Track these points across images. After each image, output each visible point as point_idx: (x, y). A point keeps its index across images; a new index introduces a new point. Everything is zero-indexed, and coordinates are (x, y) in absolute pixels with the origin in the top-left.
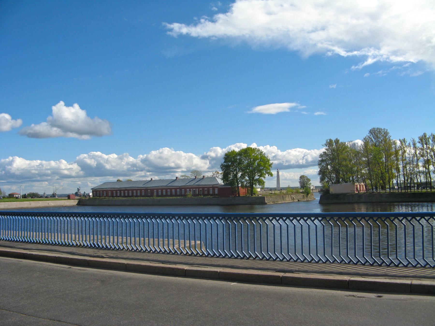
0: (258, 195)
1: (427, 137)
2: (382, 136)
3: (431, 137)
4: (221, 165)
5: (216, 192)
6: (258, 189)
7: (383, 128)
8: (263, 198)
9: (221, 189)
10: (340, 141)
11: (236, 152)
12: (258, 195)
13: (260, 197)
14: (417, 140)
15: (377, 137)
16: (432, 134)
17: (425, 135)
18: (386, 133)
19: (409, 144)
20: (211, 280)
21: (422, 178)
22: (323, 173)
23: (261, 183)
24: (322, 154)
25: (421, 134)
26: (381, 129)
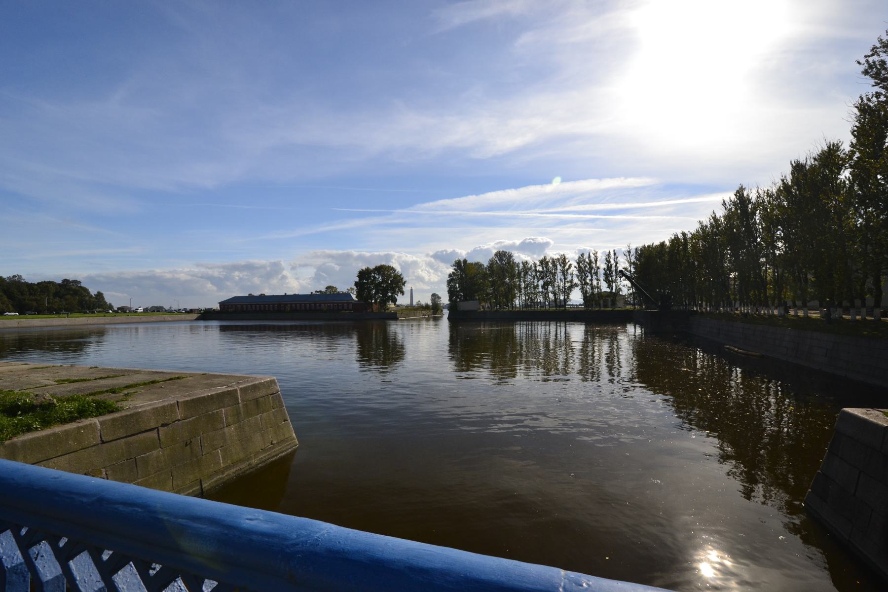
0: (391, 311)
1: (547, 260)
2: (506, 258)
3: (551, 261)
4: (881, 41)
5: (351, 307)
6: (391, 305)
7: (508, 252)
8: (395, 314)
9: (355, 304)
10: (468, 262)
11: (370, 269)
12: (391, 311)
13: (393, 313)
14: (538, 263)
15: (501, 259)
16: (551, 258)
17: (545, 259)
18: (511, 256)
19: (581, 255)
20: (262, 296)
21: (541, 298)
22: (452, 292)
23: (394, 300)
24: (850, 172)
25: (542, 257)
26: (506, 252)
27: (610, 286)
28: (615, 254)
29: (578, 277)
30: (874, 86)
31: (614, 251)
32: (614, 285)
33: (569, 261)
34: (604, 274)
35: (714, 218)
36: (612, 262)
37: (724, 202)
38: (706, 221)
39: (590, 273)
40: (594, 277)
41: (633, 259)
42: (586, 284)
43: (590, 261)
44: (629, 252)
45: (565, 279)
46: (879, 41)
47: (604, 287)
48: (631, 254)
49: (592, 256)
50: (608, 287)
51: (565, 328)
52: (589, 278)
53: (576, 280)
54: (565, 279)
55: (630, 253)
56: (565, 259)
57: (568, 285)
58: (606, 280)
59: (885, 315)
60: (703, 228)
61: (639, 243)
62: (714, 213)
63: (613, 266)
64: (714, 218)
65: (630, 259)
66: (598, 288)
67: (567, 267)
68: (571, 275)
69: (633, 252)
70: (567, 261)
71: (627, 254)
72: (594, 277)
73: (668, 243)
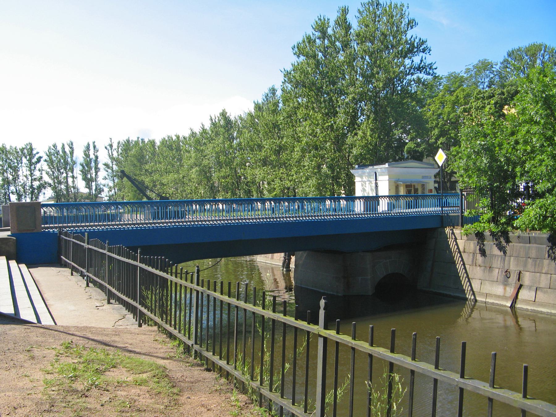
27: (89, 186)
28: (95, 147)
29: (47, 173)
30: (292, 64)
31: (94, 143)
32: (94, 184)
33: (38, 153)
34: (81, 171)
35: (203, 129)
36: (92, 156)
37: (211, 117)
38: (197, 130)
39: (65, 169)
40: (70, 174)
41: (115, 154)
42: (60, 183)
43: (64, 152)
44: (111, 146)
45: (31, 175)
46: (294, 54)
47: (82, 187)
48: (113, 148)
49: (67, 149)
50: (86, 187)
51: (387, 196)
52: (65, 175)
53: (46, 178)
54: (31, 175)
55: (112, 147)
56: (32, 149)
57: (36, 184)
58: (85, 179)
59: (555, 221)
60: (193, 134)
61: (120, 137)
62: (203, 125)
63: (92, 160)
64: (203, 129)
65: (112, 155)
66: (74, 188)
67: (34, 160)
68: (39, 170)
69: (115, 146)
70: (34, 152)
71: (108, 147)
72: (70, 174)
73: (158, 143)
